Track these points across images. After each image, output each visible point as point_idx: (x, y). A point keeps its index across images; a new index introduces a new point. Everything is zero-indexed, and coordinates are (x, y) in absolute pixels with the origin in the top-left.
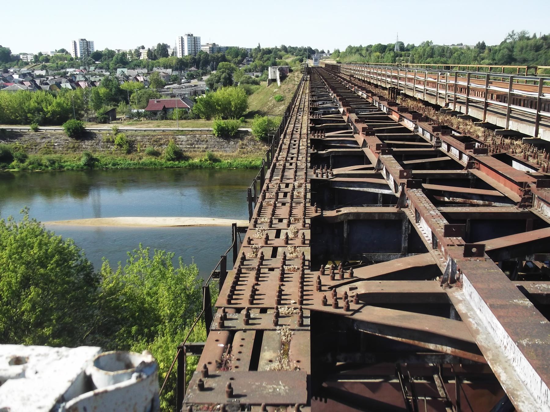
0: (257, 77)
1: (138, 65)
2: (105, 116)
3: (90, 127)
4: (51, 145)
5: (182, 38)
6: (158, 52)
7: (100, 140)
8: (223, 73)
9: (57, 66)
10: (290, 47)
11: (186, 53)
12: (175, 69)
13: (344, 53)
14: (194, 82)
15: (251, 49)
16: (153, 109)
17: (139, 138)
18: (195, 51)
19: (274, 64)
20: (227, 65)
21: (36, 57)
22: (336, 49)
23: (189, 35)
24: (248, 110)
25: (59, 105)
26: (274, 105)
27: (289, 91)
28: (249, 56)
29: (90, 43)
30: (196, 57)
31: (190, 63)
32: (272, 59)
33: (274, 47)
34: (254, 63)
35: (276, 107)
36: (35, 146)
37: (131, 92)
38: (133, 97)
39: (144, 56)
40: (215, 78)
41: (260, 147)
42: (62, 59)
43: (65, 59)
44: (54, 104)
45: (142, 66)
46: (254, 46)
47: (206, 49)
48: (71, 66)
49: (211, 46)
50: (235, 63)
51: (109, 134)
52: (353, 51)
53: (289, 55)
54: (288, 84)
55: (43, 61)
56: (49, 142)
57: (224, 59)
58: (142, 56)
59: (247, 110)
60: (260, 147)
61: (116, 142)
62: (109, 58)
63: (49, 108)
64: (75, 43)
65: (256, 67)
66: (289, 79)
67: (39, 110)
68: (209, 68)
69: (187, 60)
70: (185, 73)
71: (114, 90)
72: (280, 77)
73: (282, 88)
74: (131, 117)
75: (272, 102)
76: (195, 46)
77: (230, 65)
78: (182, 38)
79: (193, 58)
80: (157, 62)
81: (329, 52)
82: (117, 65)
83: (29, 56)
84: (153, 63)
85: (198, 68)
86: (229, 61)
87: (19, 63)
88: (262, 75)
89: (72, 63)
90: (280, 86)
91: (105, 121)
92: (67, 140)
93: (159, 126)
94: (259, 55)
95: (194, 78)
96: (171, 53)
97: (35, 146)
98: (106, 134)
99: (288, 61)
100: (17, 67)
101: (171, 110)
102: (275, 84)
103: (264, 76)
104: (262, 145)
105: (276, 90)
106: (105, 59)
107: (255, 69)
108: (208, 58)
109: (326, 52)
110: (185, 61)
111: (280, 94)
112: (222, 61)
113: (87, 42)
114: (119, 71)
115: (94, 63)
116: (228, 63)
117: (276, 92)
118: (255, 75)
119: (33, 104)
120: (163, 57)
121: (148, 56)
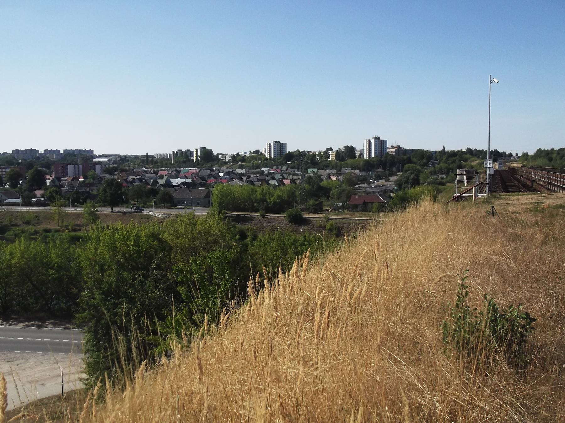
0: (442, 178)
1: (327, 165)
2: (315, 207)
3: (306, 215)
4: (275, 228)
6: (346, 154)
7: (314, 226)
8: (411, 174)
9: (253, 166)
10: (475, 150)
12: (362, 170)
13: (532, 156)
14: (382, 182)
15: (436, 152)
16: (356, 202)
17: (345, 225)
18: (381, 153)
19: (460, 167)
20: (413, 167)
22: (525, 152)
25: (279, 197)
28: (434, 158)
30: (382, 159)
32: (457, 162)
33: (459, 150)
34: (439, 166)
36: (263, 228)
37: (330, 189)
38: (332, 193)
42: (256, 159)
43: (260, 159)
44: (275, 196)
45: (331, 167)
49: (396, 148)
50: (420, 165)
51: (321, 221)
52: (543, 154)
53: (475, 158)
56: (273, 226)
57: (409, 161)
61: (327, 227)
63: (272, 199)
65: (441, 169)
67: (264, 200)
68: (394, 169)
69: (374, 161)
70: (372, 174)
71: (315, 186)
74: (336, 209)
77: (416, 167)
79: (380, 160)
80: (345, 163)
81: (517, 154)
82: (308, 166)
83: (227, 157)
84: (341, 164)
85: (384, 169)
86: (415, 163)
87: (220, 162)
88: (447, 177)
89: (267, 162)
91: (315, 212)
92: (287, 225)
93: (361, 217)
94: (444, 158)
95: (381, 179)
96: (358, 155)
97: (263, 228)
98: (319, 221)
99: (474, 164)
100: (217, 166)
101: (370, 204)
102: (462, 184)
103: (449, 178)
107: (440, 171)
109: (514, 155)
110: (371, 162)
112: (408, 163)
114: (310, 170)
116: (414, 165)
118: (440, 177)
119: (259, 196)
121: (336, 157)
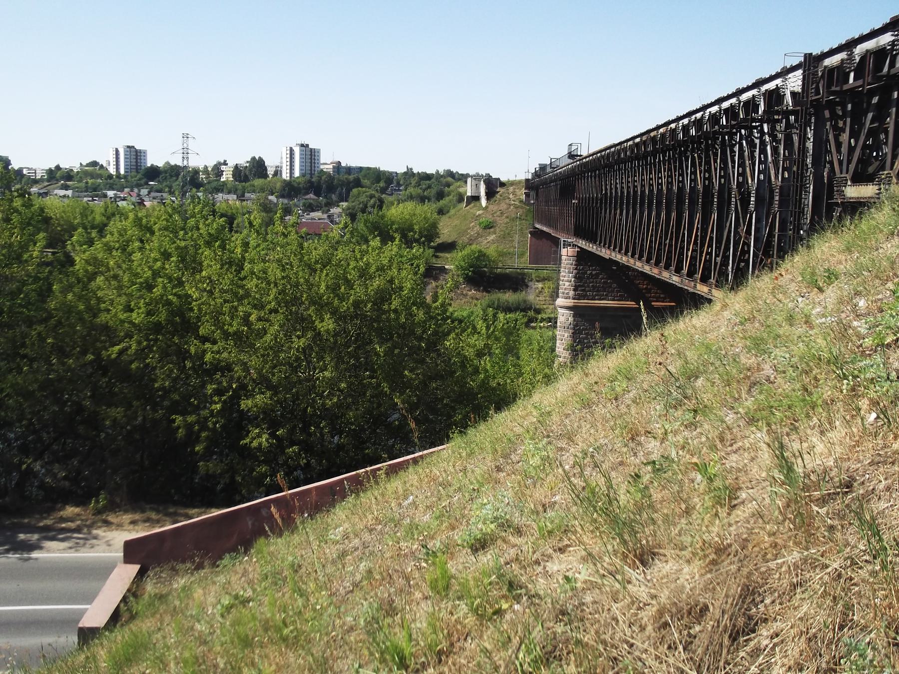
1: (221, 188)
5: (291, 150)
11: (297, 174)
21: (50, 172)
23: (302, 145)
24: (439, 241)
26: (478, 234)
27: (502, 213)
29: (140, 152)
31: (304, 188)
35: (481, 237)
39: (227, 175)
40: (359, 204)
41: (464, 292)
42: (92, 175)
46: (401, 170)
47: (328, 168)
48: (110, 187)
54: (499, 204)
55: (62, 178)
58: (224, 176)
59: (437, 240)
60: (464, 292)
62: (171, 176)
64: (117, 151)
66: (501, 196)
69: (299, 183)
72: (486, 193)
73: (489, 209)
75: (475, 229)
76: (311, 163)
78: (291, 150)
84: (243, 187)
89: (112, 181)
90: (487, 207)
96: (272, 173)
102: (477, 203)
104: (467, 289)
105: (481, 212)
106: (166, 178)
108: (332, 182)
111: (487, 218)
113: (136, 151)
115: (147, 184)
117: (479, 215)
120: (259, 177)
121: (234, 176)
